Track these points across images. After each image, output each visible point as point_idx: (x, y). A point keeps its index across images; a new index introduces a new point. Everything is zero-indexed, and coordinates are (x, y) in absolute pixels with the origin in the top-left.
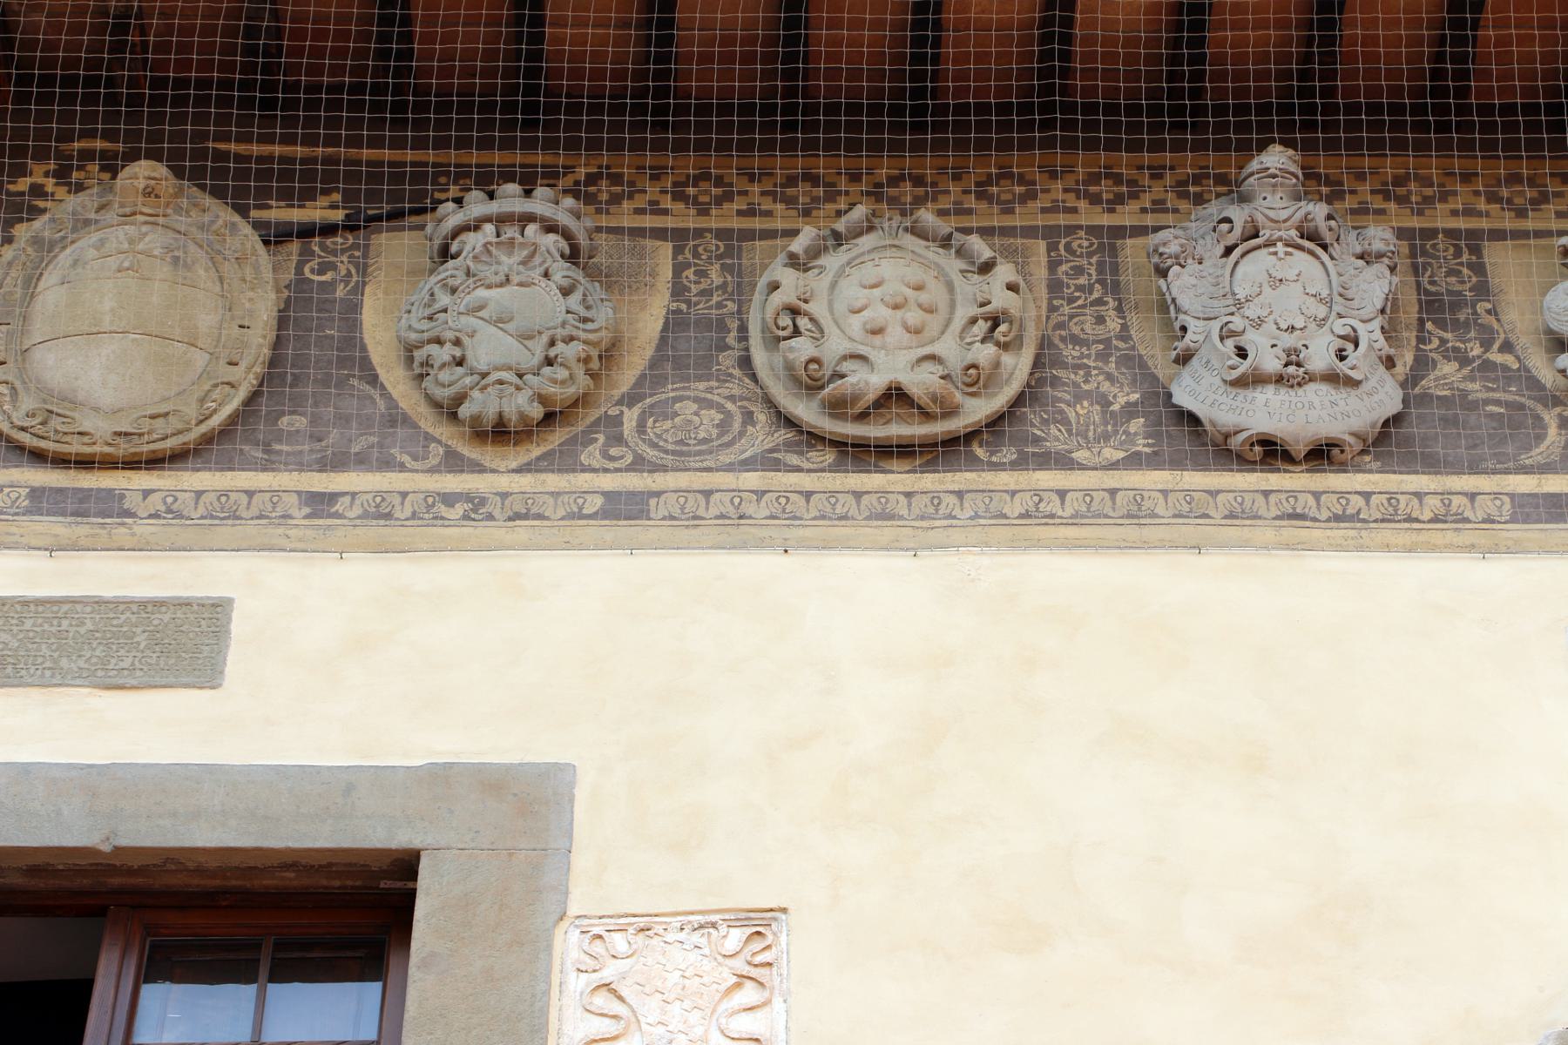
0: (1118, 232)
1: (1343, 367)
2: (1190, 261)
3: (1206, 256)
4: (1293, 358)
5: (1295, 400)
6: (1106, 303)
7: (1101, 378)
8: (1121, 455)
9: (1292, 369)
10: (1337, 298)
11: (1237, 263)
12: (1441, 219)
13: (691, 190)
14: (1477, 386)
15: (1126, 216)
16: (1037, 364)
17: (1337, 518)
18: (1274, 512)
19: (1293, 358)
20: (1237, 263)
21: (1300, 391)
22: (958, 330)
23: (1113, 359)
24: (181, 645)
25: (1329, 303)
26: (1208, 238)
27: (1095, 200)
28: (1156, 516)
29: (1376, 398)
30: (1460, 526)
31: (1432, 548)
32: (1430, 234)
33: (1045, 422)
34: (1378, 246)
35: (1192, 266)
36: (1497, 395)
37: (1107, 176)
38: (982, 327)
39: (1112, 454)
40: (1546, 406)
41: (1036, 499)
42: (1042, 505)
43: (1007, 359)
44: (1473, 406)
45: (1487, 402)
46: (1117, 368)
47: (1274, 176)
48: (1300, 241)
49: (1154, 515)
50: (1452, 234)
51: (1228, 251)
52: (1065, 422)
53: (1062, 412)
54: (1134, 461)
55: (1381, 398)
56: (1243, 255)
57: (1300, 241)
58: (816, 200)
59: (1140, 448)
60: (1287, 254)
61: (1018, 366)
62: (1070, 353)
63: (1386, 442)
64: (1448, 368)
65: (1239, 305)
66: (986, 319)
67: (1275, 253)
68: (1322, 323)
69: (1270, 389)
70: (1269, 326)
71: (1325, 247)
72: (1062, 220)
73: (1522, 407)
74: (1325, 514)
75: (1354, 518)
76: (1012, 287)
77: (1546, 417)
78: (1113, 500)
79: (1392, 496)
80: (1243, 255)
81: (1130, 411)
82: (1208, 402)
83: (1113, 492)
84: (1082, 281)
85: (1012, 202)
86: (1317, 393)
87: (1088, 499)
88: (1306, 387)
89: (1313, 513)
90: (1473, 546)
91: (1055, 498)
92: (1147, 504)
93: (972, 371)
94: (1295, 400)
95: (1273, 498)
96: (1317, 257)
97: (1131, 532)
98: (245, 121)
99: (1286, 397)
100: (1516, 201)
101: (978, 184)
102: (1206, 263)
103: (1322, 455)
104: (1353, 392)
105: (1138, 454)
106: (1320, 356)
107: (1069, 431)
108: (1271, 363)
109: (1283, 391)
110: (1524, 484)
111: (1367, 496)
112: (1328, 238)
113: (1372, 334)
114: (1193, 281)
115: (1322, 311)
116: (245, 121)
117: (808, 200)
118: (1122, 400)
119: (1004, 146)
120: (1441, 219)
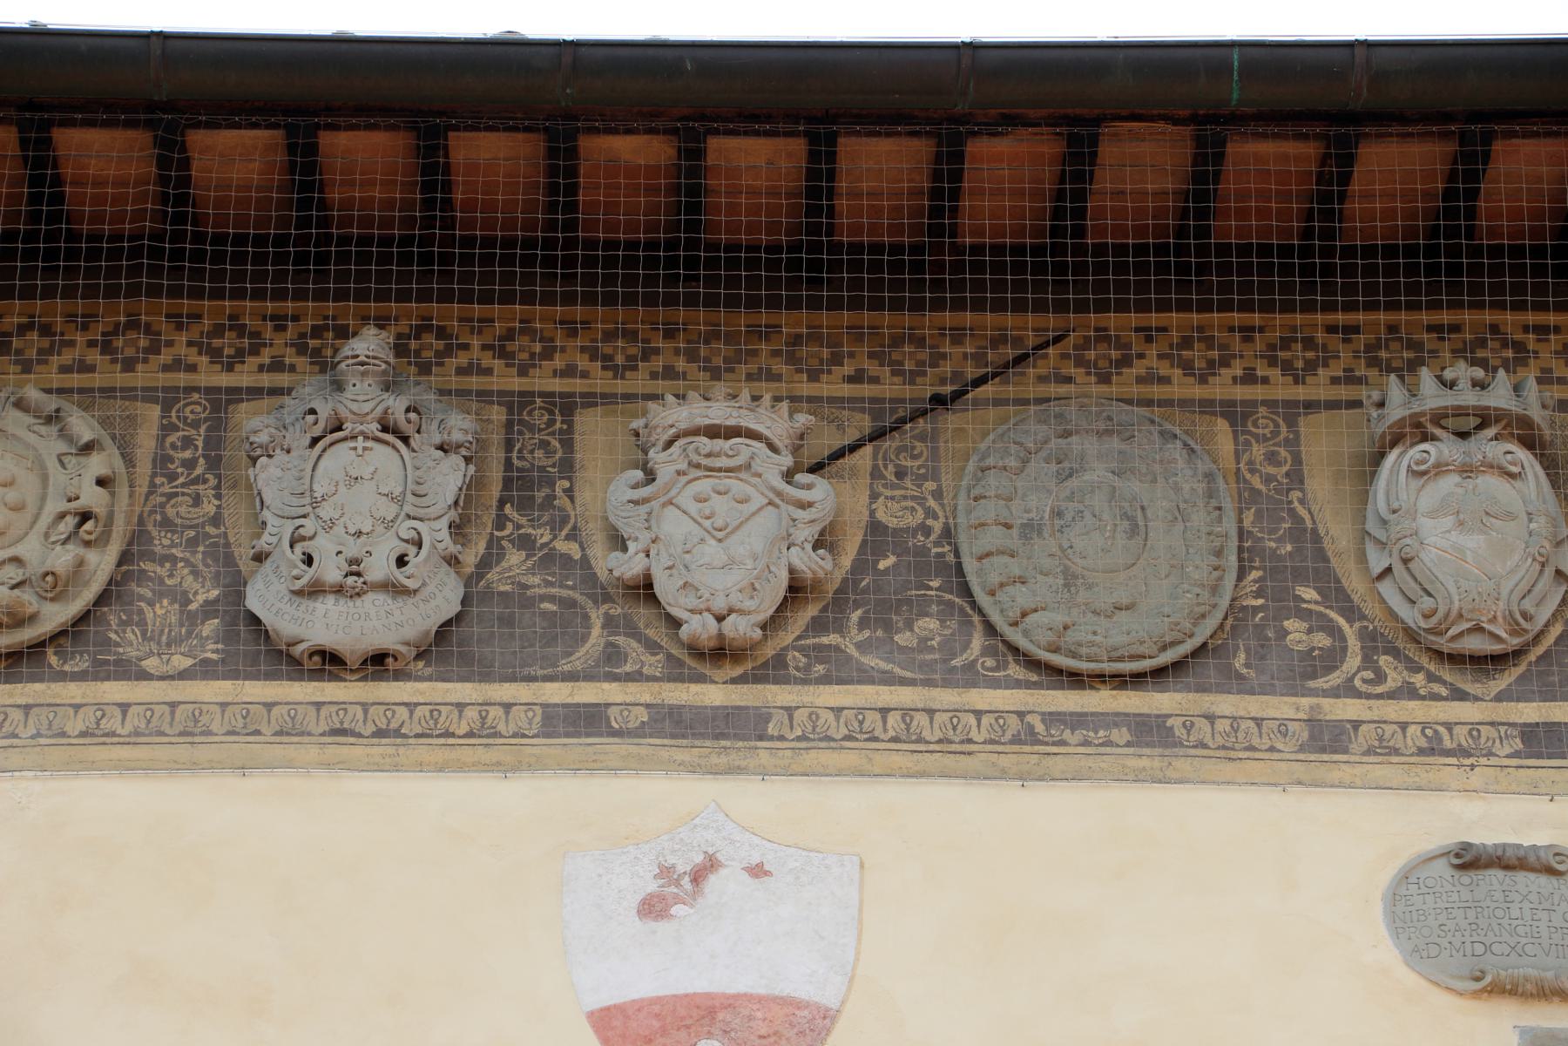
0: (236, 394)
1: (399, 575)
2: (278, 451)
3: (294, 445)
4: (354, 567)
5: (352, 611)
6: (205, 481)
7: (186, 571)
8: (189, 662)
9: (351, 580)
10: (409, 497)
11: (320, 457)
12: (544, 381)
14: (536, 580)
15: (244, 377)
16: (124, 558)
17: (380, 733)
18: (323, 727)
19: (354, 567)
20: (320, 457)
21: (358, 602)
22: (44, 529)
23: (201, 549)
25: (399, 501)
26: (298, 426)
27: (215, 354)
28: (210, 733)
29: (433, 603)
30: (491, 741)
31: (461, 767)
32: (526, 397)
33: (123, 623)
34: (457, 436)
35: (280, 456)
36: (554, 591)
37: (231, 328)
38: (71, 521)
39: (181, 662)
40: (595, 602)
41: (99, 714)
42: (103, 721)
43: (92, 556)
44: (529, 603)
45: (543, 598)
46: (204, 560)
47: (362, 364)
48: (381, 435)
49: (209, 733)
51: (315, 441)
52: (142, 623)
53: (141, 612)
54: (205, 670)
55: (442, 598)
56: (332, 444)
57: (381, 435)
59: (209, 655)
60: (365, 449)
61: (102, 563)
62: (161, 542)
63: (442, 648)
64: (514, 557)
65: (315, 504)
66: (76, 514)
67: (355, 449)
68: (389, 524)
69: (330, 599)
70: (339, 529)
71: (405, 440)
72: (182, 378)
73: (573, 604)
74: (371, 729)
75: (397, 733)
76: (101, 482)
77: (593, 616)
78: (173, 713)
79: (435, 708)
80: (324, 450)
81: (209, 610)
82: (274, 610)
83: (173, 705)
84: (187, 454)
86: (375, 603)
87: (149, 713)
88: (364, 597)
89: (359, 728)
90: (499, 763)
91: (117, 712)
92: (204, 719)
93: (49, 578)
94: (352, 611)
95: (324, 711)
96: (394, 447)
97: (183, 752)
99: (344, 609)
102: (293, 453)
103: (378, 663)
104: (410, 601)
105: (205, 662)
106: (379, 566)
107: (144, 633)
108: (331, 571)
109: (342, 601)
110: (557, 693)
111: (411, 706)
112: (409, 430)
113: (437, 534)
114: (278, 473)
115: (389, 510)
118: (201, 598)
119: (133, 291)
120: (544, 381)
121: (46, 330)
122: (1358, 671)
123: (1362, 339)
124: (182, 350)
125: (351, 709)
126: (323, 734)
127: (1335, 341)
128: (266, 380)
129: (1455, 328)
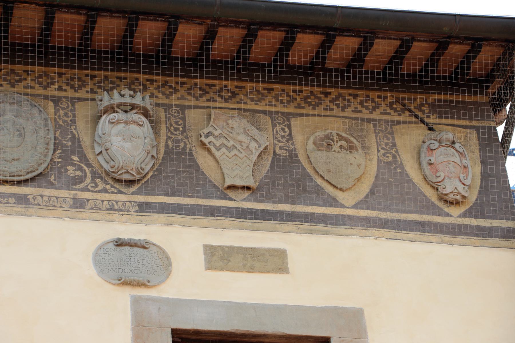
13: (103, 85)
24: (274, 262)
31: (172, 224)
37: (45, 76)
50: (177, 106)
58: (48, 83)
85: (228, 99)
98: (151, 68)
100: (12, 81)
101: (4, 75)
116: (151, 68)
117: (46, 84)
121: (80, 79)
122: (90, 183)
123: (186, 87)
124: (29, 81)
125: (52, 199)
126: (134, 212)
127: (178, 86)
128: (323, 113)
129: (125, 78)
